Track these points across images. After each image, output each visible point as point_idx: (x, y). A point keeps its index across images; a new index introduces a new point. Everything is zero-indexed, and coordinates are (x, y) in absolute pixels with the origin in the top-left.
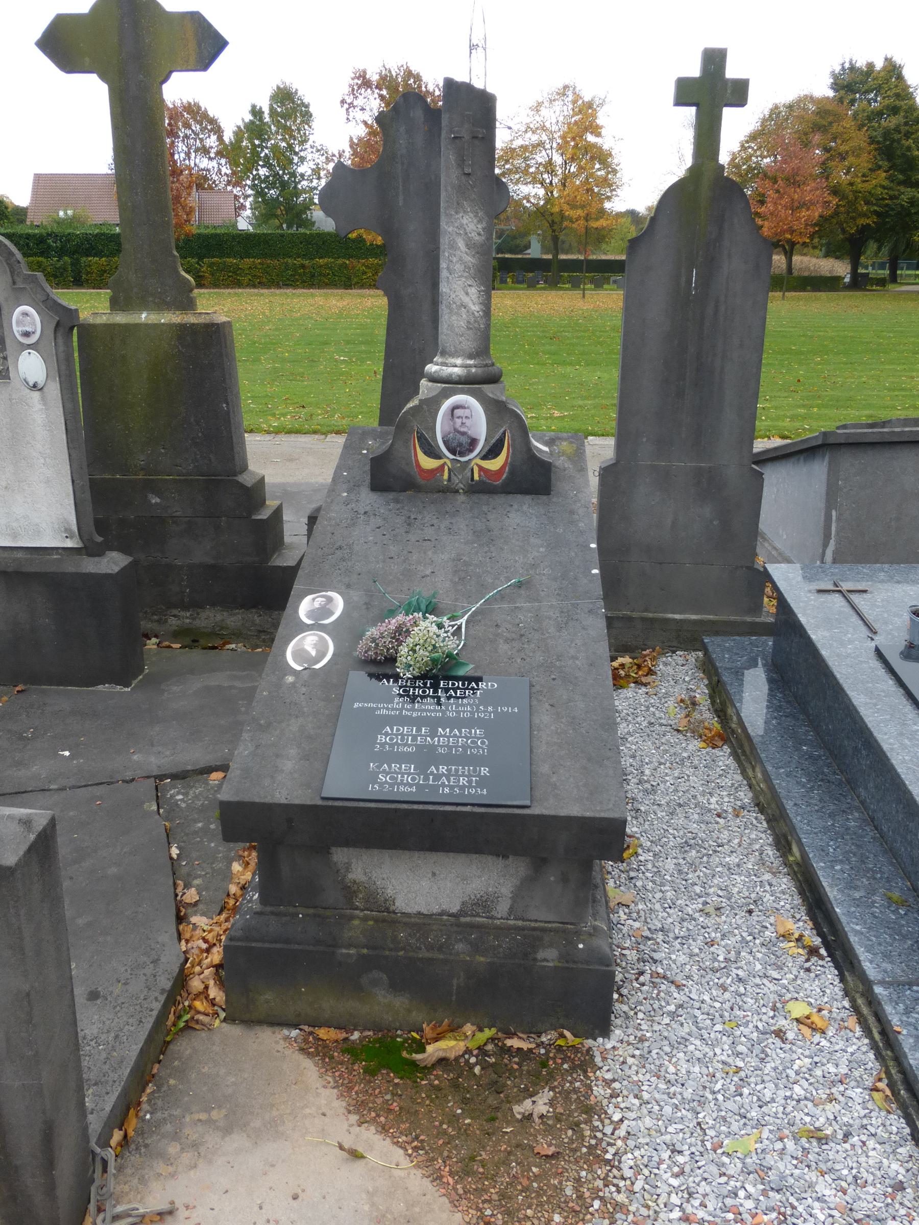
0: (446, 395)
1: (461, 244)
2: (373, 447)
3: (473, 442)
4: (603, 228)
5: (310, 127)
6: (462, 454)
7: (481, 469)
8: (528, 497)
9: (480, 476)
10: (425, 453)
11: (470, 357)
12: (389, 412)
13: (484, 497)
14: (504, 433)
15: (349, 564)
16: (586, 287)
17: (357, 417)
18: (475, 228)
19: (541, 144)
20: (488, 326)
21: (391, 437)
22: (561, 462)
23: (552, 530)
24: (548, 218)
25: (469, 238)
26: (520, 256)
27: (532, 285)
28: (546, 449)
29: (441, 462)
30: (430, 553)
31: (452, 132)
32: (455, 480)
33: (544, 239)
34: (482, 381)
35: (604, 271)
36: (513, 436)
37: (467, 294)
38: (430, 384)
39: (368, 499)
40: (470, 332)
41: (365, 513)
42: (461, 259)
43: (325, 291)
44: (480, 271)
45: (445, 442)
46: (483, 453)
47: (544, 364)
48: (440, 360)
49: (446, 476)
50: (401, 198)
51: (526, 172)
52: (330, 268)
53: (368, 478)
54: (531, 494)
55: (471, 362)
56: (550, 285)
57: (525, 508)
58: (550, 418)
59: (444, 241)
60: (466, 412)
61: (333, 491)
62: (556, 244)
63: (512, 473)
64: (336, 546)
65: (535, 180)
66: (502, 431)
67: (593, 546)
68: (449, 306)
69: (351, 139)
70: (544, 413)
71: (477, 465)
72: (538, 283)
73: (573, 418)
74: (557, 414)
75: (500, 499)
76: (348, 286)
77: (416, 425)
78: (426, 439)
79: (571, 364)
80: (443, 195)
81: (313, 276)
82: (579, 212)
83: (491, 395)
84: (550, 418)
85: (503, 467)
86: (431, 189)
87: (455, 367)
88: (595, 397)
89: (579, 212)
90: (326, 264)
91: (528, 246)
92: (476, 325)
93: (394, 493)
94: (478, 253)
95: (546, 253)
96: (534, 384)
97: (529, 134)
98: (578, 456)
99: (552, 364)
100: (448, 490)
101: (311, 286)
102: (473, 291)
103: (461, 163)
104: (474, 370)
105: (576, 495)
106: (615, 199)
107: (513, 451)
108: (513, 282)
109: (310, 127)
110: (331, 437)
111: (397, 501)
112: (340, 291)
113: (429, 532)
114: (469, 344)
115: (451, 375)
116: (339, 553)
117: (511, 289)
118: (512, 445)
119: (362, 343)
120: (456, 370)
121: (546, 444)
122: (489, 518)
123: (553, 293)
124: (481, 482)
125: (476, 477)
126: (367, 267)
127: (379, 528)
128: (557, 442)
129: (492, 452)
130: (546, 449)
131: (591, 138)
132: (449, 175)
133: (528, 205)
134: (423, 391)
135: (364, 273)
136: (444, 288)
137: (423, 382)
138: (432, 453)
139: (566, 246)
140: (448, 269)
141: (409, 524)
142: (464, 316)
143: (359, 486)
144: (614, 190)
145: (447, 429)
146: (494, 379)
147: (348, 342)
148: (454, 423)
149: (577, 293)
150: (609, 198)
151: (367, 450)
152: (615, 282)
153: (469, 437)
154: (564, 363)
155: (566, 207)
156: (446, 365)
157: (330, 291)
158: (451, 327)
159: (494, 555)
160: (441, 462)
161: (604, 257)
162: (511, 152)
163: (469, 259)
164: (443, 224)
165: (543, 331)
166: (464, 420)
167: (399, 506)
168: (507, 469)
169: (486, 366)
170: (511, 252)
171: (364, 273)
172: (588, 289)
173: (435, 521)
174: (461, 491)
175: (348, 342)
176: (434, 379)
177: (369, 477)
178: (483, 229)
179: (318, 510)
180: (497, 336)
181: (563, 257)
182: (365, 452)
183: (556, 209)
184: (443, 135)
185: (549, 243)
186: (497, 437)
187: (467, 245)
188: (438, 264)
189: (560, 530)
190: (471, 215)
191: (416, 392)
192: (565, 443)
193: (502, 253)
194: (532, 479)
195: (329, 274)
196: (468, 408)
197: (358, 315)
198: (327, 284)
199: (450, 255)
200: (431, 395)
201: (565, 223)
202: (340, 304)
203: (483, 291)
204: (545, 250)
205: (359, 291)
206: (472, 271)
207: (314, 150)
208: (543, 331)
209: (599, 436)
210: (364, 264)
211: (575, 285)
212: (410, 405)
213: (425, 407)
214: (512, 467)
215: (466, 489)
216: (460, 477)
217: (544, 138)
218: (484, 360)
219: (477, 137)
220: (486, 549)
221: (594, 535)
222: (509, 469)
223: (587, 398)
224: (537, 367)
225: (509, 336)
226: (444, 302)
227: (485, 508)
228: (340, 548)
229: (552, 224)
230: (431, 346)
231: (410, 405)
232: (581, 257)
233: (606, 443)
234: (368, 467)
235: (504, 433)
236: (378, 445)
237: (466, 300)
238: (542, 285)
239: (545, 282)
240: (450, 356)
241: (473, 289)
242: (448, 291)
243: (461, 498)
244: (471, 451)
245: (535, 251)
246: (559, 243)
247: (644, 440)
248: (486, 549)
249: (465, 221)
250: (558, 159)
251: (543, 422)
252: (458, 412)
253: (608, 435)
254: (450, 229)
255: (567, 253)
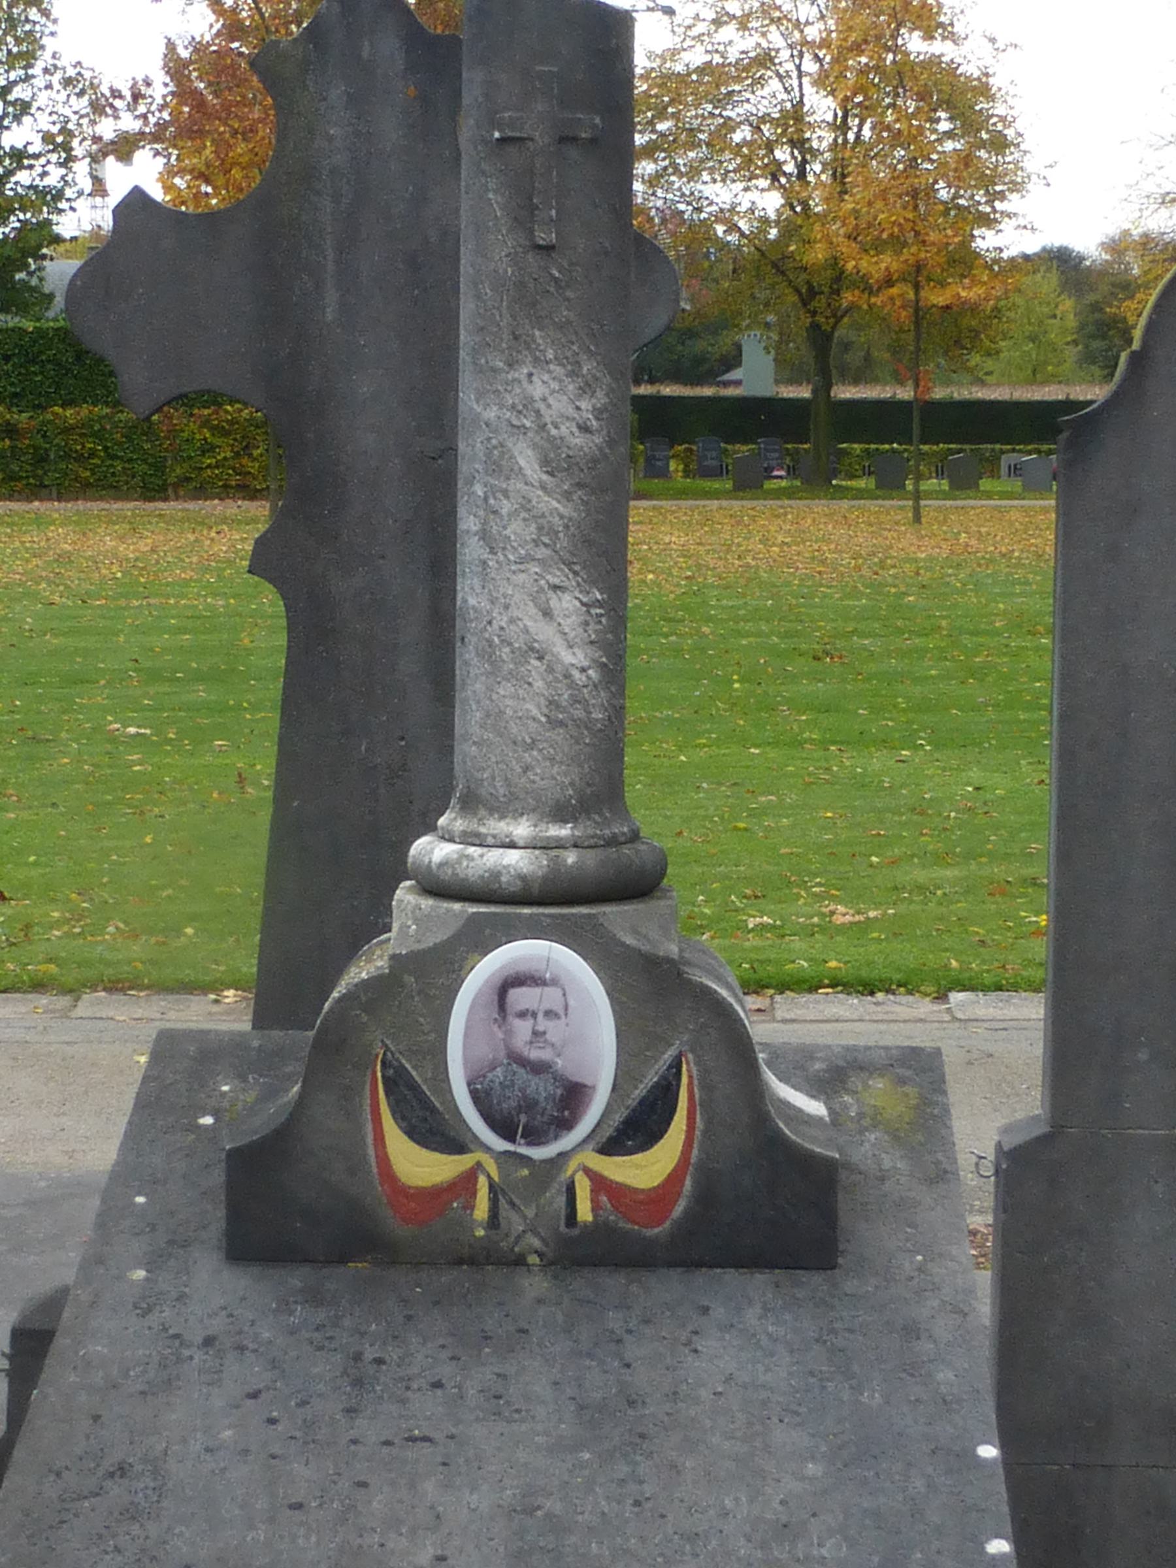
0: (479, 938)
1: (526, 459)
2: (236, 1106)
3: (574, 1095)
4: (973, 308)
5: (46, 13)
6: (534, 1136)
7: (599, 1183)
8: (761, 1278)
9: (596, 1207)
10: (413, 1133)
11: (560, 814)
12: (286, 990)
13: (614, 1282)
14: (676, 1065)
15: (153, 1529)
16: (925, 486)
17: (179, 933)
18: (571, 411)
19: (765, 59)
20: (617, 713)
21: (295, 1067)
22: (870, 1151)
23: (846, 1396)
24: (793, 280)
25: (551, 440)
26: (708, 391)
27: (749, 483)
28: (815, 1108)
29: (464, 1162)
30: (429, 1487)
31: (495, 124)
32: (515, 1223)
33: (785, 337)
34: (601, 891)
35: (976, 437)
36: (705, 1072)
37: (547, 613)
38: (427, 903)
39: (215, 1290)
40: (559, 735)
41: (209, 1342)
42: (526, 505)
43: (80, 505)
44: (588, 542)
45: (476, 1097)
46: (608, 1132)
47: (798, 743)
48: (459, 825)
49: (481, 1210)
50: (331, 297)
51: (719, 139)
52: (99, 436)
53: (217, 1216)
54: (771, 1265)
55: (563, 831)
56: (807, 481)
57: (751, 1316)
58: (822, 929)
59: (471, 451)
60: (549, 997)
61: (100, 1261)
62: (822, 353)
63: (705, 1197)
64: (108, 1464)
65: (755, 163)
66: (669, 1055)
67: (988, 1452)
68: (488, 653)
69: (171, 46)
70: (802, 911)
71: (587, 1171)
72: (768, 474)
73: (898, 929)
74: (843, 915)
75: (667, 1287)
76: (155, 488)
77: (379, 1042)
78: (414, 1087)
79: (884, 743)
80: (467, 309)
81: (41, 459)
82: (887, 261)
83: (629, 940)
84: (822, 929)
85: (674, 1179)
86: (428, 278)
87: (511, 850)
88: (970, 856)
89: (887, 261)
90: (86, 424)
91: (733, 360)
92: (579, 713)
93: (306, 1270)
94: (580, 485)
95: (791, 381)
96: (764, 811)
97: (729, 32)
98: (927, 1124)
99: (824, 744)
100: (492, 1258)
101: (37, 490)
102: (567, 604)
103: (524, 214)
104: (571, 858)
105: (920, 1269)
106: (1007, 225)
107: (709, 1122)
108: (687, 473)
109: (46, 13)
110: (92, 1004)
111: (314, 1297)
112: (128, 507)
113: (427, 1408)
114: (553, 774)
115: (495, 875)
116: (116, 1490)
117: (682, 494)
118: (705, 1105)
119: (198, 677)
120: (512, 858)
121: (818, 1087)
122: (628, 1356)
123: (820, 506)
124: (600, 1228)
125: (584, 1212)
126: (218, 430)
127: (254, 1395)
128: (855, 1082)
129: (637, 1128)
130: (815, 1108)
131: (915, 44)
132: (486, 254)
133: (733, 238)
134: (404, 927)
135: (208, 449)
136: (470, 594)
137: (405, 895)
138: (435, 1130)
139: (854, 358)
140: (484, 535)
141: (358, 1383)
142: (539, 684)
143: (185, 1244)
144: (1001, 196)
145: (485, 1052)
146: (639, 885)
147: (153, 676)
148: (509, 1033)
149: (896, 508)
150: (987, 221)
151: (216, 1113)
152: (1015, 470)
153: (558, 1078)
154: (861, 741)
155: (846, 248)
156: (479, 841)
157: (95, 506)
158: (495, 717)
159: (648, 1490)
160: (464, 1162)
161: (980, 394)
162: (676, 86)
163: (554, 507)
164: (468, 399)
165: (787, 635)
166: (543, 1024)
167: (321, 1315)
168: (688, 1182)
169: (612, 842)
170: (676, 376)
171: (208, 449)
172: (930, 495)
173: (446, 1371)
174: (533, 1259)
175: (153, 676)
176: (439, 887)
177: (221, 1212)
178: (598, 413)
179: (53, 1304)
180: (640, 652)
181: (845, 392)
182: (208, 1120)
183: (818, 254)
184: (467, 130)
185: (800, 349)
186: (652, 1078)
187: (545, 462)
188: (449, 517)
189: (872, 1398)
190: (558, 370)
191: (376, 919)
192: (878, 1084)
193: (652, 381)
194: (773, 1214)
195: (93, 454)
196: (554, 982)
197: (186, 583)
198: (87, 485)
199: (492, 491)
200: (430, 941)
201: (848, 297)
202: (127, 550)
203: (599, 604)
204: (788, 371)
205: (191, 505)
206: (563, 542)
207: (56, 79)
208: (787, 635)
209: (985, 989)
210: (206, 423)
211: (890, 480)
212: (360, 972)
213: (409, 979)
214: (706, 1177)
215: (550, 1255)
216: (530, 1213)
217: (775, 38)
218: (607, 823)
219: (575, 139)
220: (623, 1469)
221: (988, 1409)
222: (696, 1183)
223: (939, 859)
224: (772, 753)
225: (677, 651)
226: (471, 639)
227: (614, 1320)
228: (122, 1470)
229: (808, 296)
230: (425, 784)
231: (360, 972)
232: (905, 393)
233: (1010, 1012)
234: (217, 1177)
235: (676, 1065)
236: (251, 1097)
237: (543, 632)
238: (780, 480)
239: (792, 472)
240: (492, 810)
241: (567, 597)
242: (485, 605)
243: (534, 1284)
244: (566, 1124)
245: (756, 375)
246: (834, 350)
247: (1143, 1056)
248: (623, 1469)
249: (537, 390)
250: (821, 106)
251: (797, 943)
252: (521, 997)
253: (1015, 987)
254: (491, 414)
255: (856, 381)
